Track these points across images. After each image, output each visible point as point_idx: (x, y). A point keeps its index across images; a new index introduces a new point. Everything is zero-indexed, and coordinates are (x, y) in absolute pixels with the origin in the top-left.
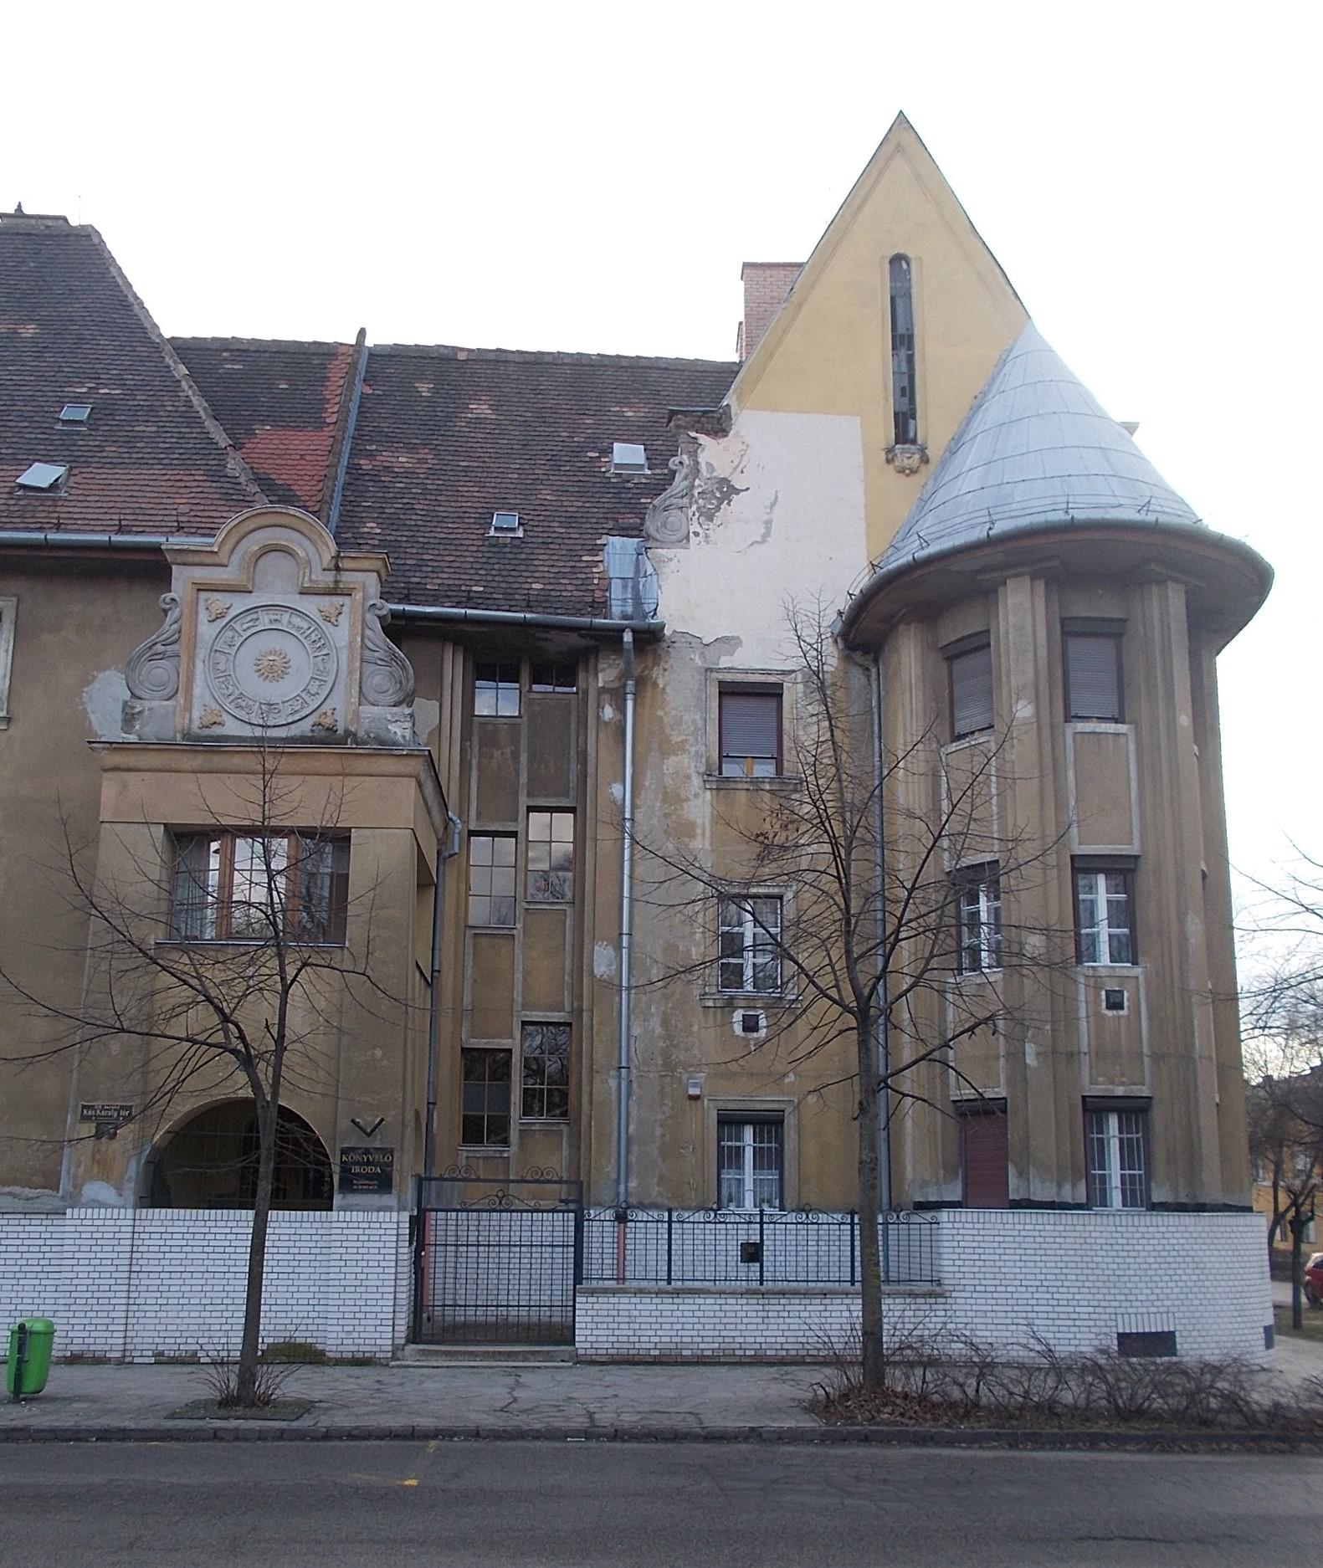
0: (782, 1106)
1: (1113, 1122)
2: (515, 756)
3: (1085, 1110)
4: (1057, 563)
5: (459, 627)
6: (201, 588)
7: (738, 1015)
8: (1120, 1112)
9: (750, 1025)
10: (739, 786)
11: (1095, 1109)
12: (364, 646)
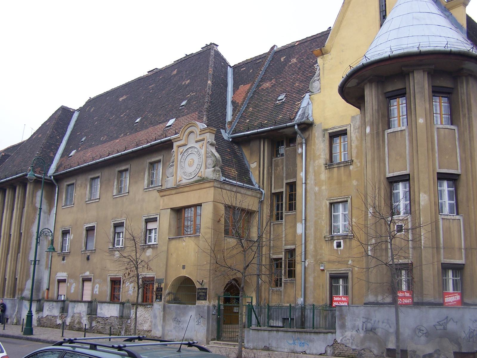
0: (347, 272)
1: (450, 273)
2: (283, 168)
3: (442, 268)
4: (371, 77)
5: (281, 131)
6: (179, 147)
7: (335, 242)
8: (453, 269)
9: (339, 245)
10: (335, 166)
11: (445, 267)
12: (206, 153)
